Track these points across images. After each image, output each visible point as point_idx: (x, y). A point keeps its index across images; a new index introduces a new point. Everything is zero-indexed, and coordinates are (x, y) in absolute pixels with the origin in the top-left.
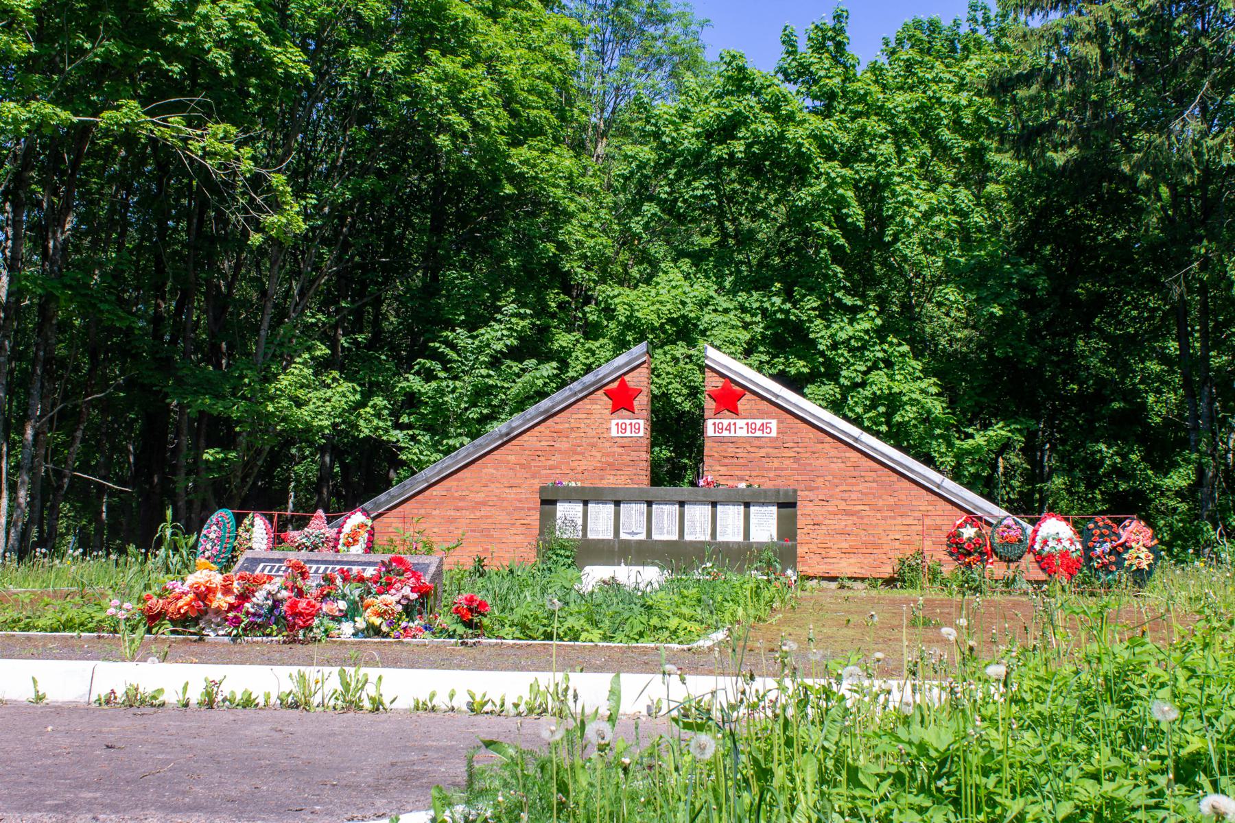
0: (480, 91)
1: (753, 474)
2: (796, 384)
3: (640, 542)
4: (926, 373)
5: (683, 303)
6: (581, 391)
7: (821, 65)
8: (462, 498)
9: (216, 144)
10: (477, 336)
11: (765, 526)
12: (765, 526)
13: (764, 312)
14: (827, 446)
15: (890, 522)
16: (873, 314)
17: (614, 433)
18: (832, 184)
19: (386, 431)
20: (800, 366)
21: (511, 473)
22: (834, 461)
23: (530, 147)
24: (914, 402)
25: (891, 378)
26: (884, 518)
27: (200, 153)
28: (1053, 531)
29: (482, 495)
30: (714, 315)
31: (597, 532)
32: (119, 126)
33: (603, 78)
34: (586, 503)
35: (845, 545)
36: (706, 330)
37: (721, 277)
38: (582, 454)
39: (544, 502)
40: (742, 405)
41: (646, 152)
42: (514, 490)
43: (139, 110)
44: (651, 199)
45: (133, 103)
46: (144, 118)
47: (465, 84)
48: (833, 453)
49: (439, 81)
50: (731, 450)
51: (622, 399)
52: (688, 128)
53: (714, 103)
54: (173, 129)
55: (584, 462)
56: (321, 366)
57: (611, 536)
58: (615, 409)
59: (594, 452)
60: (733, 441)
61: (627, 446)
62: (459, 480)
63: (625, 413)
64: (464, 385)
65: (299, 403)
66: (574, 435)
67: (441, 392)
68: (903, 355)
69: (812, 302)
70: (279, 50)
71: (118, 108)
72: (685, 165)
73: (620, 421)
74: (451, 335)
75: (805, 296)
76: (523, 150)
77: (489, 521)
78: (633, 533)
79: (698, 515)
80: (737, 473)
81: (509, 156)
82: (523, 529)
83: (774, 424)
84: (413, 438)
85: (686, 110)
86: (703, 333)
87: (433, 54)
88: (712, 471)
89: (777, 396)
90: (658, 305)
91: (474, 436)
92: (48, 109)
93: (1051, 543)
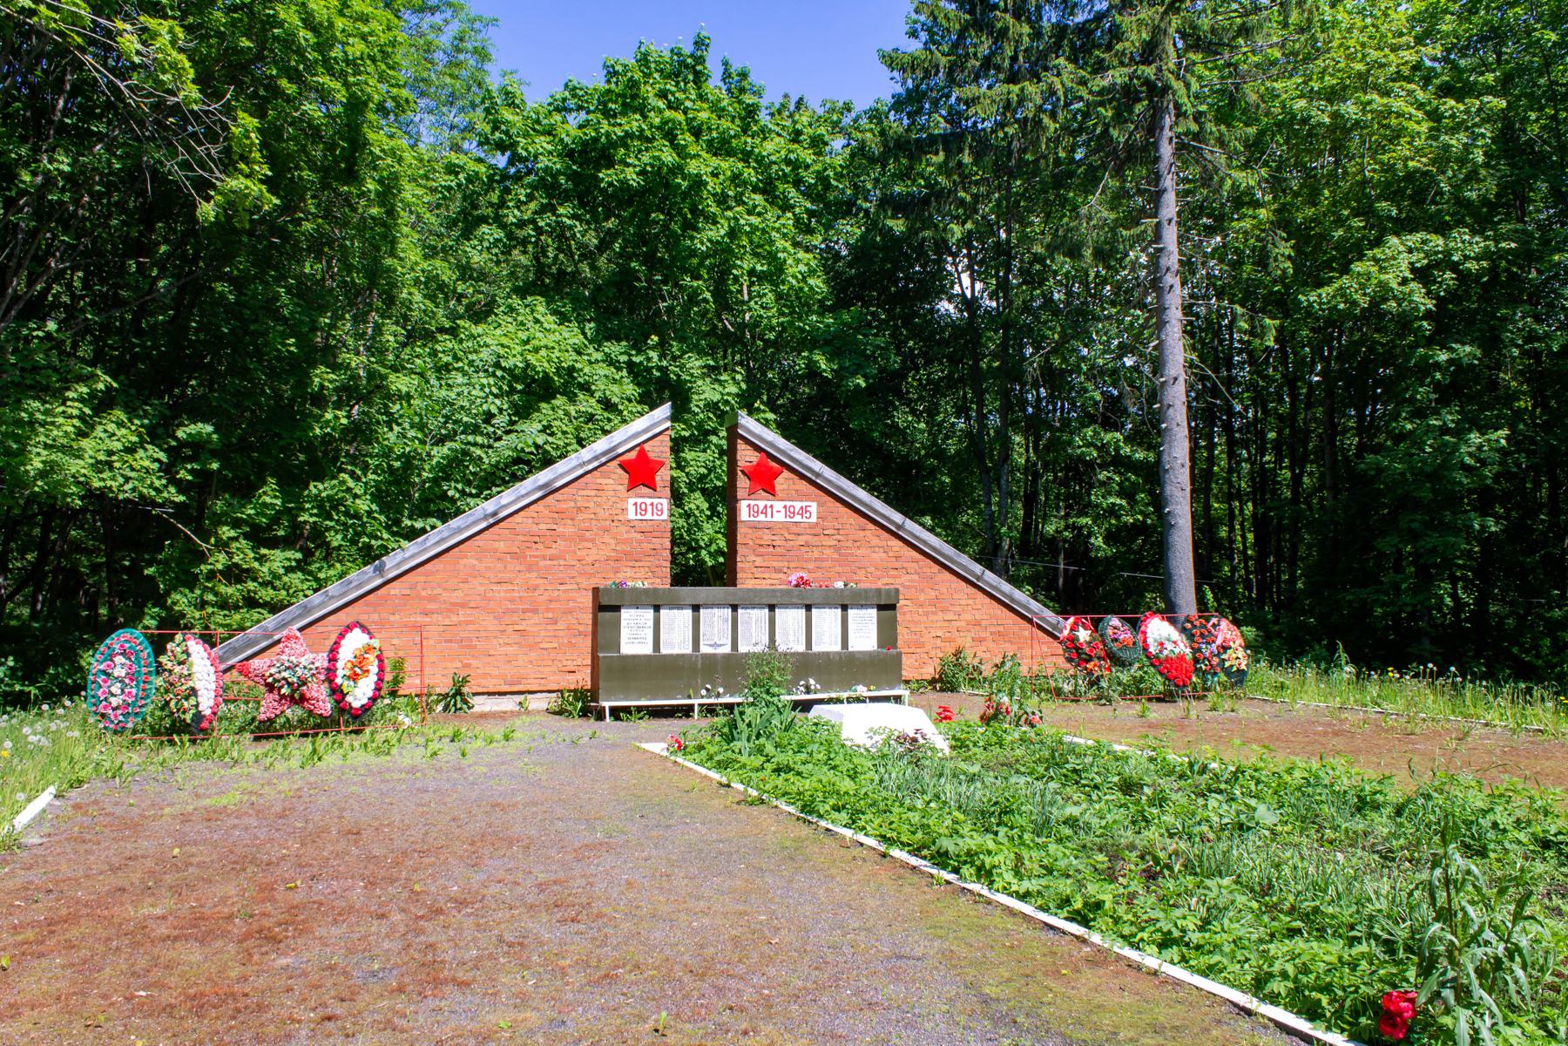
1: (792, 565)
3: (725, 656)
6: (590, 461)
8: (432, 599)
11: (864, 632)
12: (864, 632)
14: (868, 533)
15: (932, 617)
17: (631, 515)
18: (733, 233)
21: (500, 566)
26: (927, 614)
29: (459, 594)
31: (672, 645)
34: (657, 608)
38: (592, 541)
42: (505, 587)
48: (875, 541)
50: (767, 537)
55: (594, 551)
57: (688, 650)
58: (632, 485)
59: (607, 539)
60: (769, 527)
62: (427, 574)
66: (581, 516)
73: (639, 501)
75: (685, 353)
77: (471, 627)
79: (754, 622)
80: (775, 564)
82: (516, 637)
83: (813, 507)
88: (747, 580)
93: (1169, 646)
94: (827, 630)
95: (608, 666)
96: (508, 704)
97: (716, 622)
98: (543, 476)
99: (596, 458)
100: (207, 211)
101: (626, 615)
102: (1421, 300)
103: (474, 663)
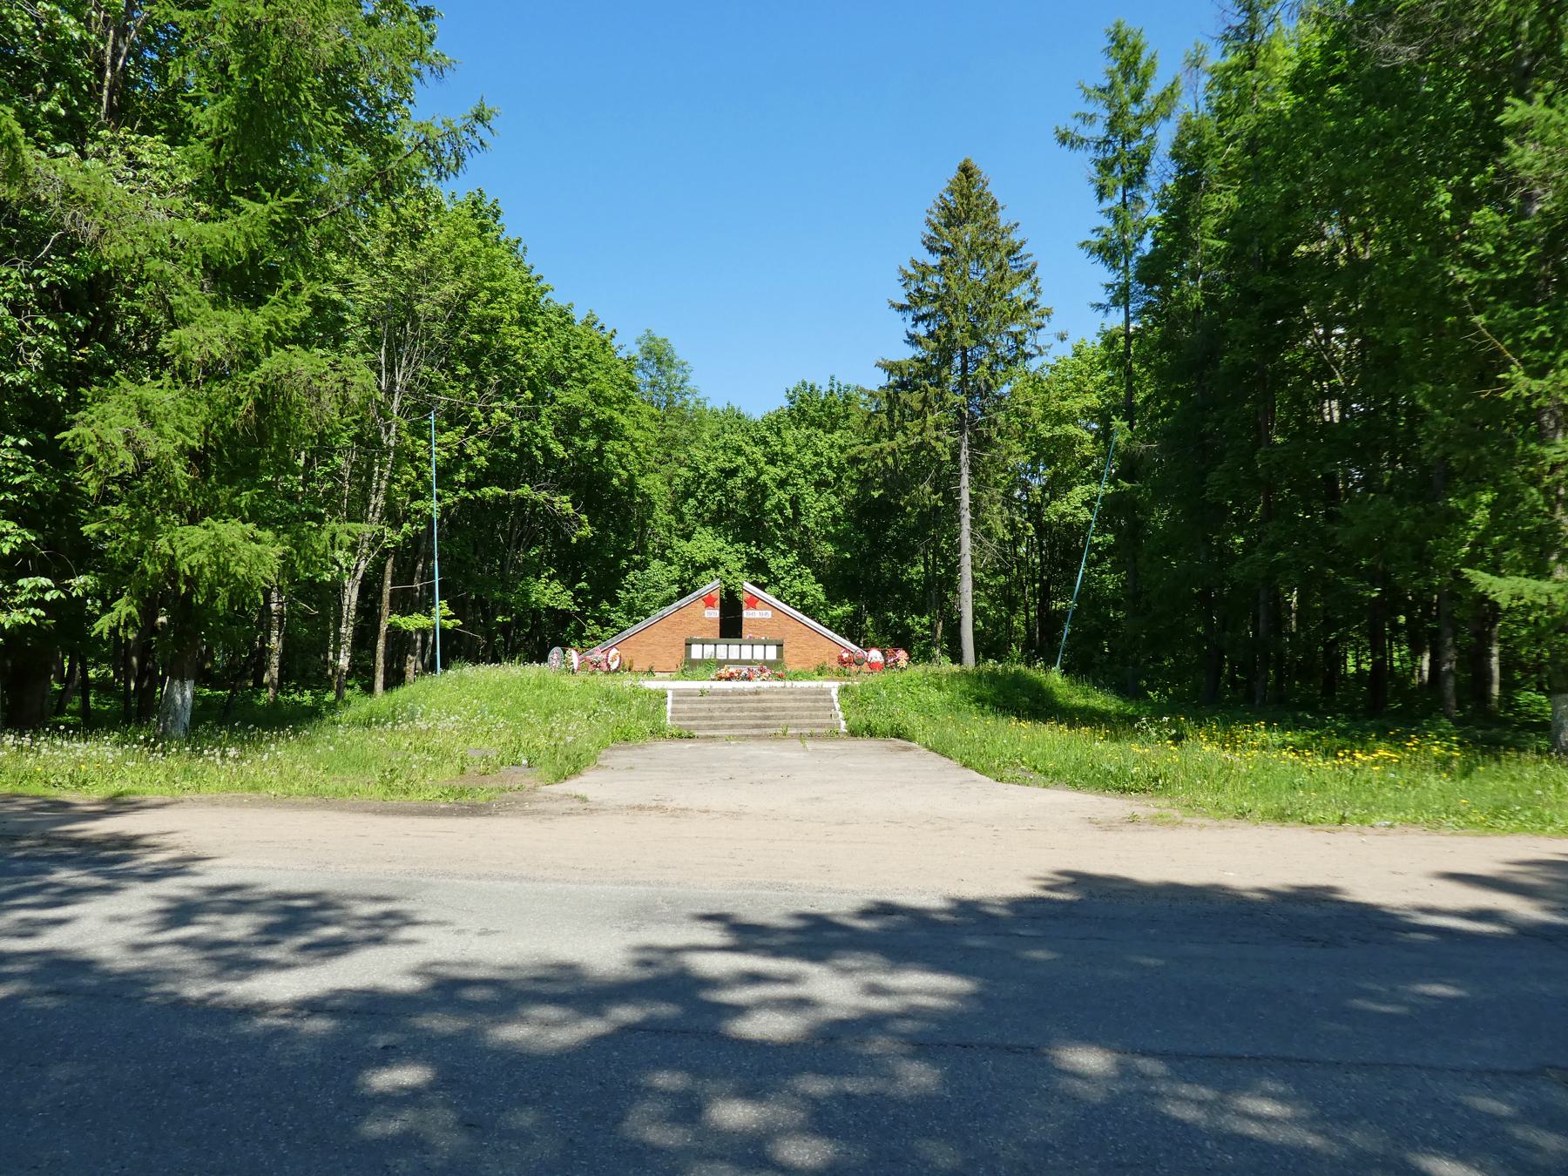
2: (762, 587)
4: (818, 582)
7: (772, 439)
11: (772, 653)
12: (772, 653)
20: (764, 579)
22: (793, 628)
51: (709, 602)
61: (712, 621)
79: (746, 650)
88: (747, 633)
91: (647, 616)
94: (759, 652)
97: (734, 649)
98: (677, 603)
100: (574, 540)
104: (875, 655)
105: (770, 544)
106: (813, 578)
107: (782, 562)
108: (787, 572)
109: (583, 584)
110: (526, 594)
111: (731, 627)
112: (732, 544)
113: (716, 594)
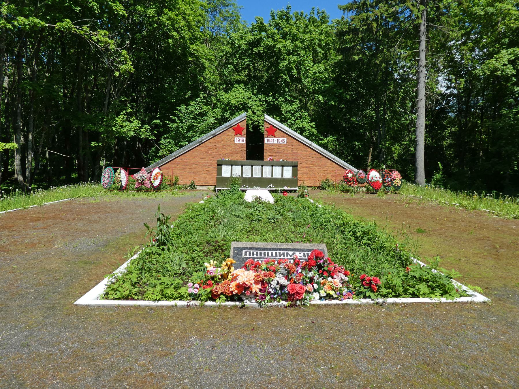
0: (181, 24)
4: (311, 121)
5: (244, 98)
7: (283, 24)
8: (186, 162)
9: (103, 38)
10: (188, 109)
11: (288, 173)
12: (288, 173)
13: (266, 101)
16: (297, 103)
17: (236, 142)
18: (290, 62)
19: (149, 136)
23: (196, 45)
24: (309, 130)
25: (302, 122)
27: (96, 41)
28: (374, 175)
30: (252, 102)
32: (64, 29)
33: (212, 25)
34: (232, 166)
35: (306, 177)
36: (251, 107)
37: (253, 89)
39: (218, 165)
40: (276, 133)
41: (227, 49)
43: (71, 23)
44: (230, 64)
45: (69, 20)
46: (73, 26)
47: (177, 23)
48: (303, 149)
49: (167, 20)
50: (272, 147)
51: (238, 131)
52: (243, 42)
53: (249, 34)
54: (84, 31)
56: (129, 115)
59: (229, 148)
60: (273, 145)
61: (240, 145)
63: (239, 135)
64: (185, 125)
65: (122, 126)
67: (177, 127)
68: (306, 116)
69: (281, 99)
70: (114, 4)
71: (63, 22)
72: (242, 53)
74: (179, 108)
76: (194, 46)
78: (247, 175)
79: (267, 170)
81: (190, 48)
83: (285, 139)
84: (169, 142)
85: (242, 36)
86: (250, 108)
87: (166, 10)
88: (268, 156)
89: (287, 131)
90: (237, 99)
91: (189, 142)
92: (36, 20)
93: (374, 179)
94: (277, 172)
95: (222, 181)
96: (205, 188)
98: (213, 132)
99: (227, 127)
100: (117, 74)
101: (223, 167)
102: (510, 70)
103: (197, 178)
104: (374, 175)
105: (283, 95)
106: (308, 118)
107: (290, 108)
108: (293, 115)
109: (158, 121)
110: (110, 126)
111: (255, 151)
112: (256, 95)
113: (243, 125)
